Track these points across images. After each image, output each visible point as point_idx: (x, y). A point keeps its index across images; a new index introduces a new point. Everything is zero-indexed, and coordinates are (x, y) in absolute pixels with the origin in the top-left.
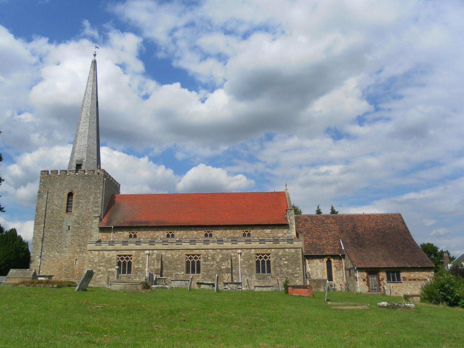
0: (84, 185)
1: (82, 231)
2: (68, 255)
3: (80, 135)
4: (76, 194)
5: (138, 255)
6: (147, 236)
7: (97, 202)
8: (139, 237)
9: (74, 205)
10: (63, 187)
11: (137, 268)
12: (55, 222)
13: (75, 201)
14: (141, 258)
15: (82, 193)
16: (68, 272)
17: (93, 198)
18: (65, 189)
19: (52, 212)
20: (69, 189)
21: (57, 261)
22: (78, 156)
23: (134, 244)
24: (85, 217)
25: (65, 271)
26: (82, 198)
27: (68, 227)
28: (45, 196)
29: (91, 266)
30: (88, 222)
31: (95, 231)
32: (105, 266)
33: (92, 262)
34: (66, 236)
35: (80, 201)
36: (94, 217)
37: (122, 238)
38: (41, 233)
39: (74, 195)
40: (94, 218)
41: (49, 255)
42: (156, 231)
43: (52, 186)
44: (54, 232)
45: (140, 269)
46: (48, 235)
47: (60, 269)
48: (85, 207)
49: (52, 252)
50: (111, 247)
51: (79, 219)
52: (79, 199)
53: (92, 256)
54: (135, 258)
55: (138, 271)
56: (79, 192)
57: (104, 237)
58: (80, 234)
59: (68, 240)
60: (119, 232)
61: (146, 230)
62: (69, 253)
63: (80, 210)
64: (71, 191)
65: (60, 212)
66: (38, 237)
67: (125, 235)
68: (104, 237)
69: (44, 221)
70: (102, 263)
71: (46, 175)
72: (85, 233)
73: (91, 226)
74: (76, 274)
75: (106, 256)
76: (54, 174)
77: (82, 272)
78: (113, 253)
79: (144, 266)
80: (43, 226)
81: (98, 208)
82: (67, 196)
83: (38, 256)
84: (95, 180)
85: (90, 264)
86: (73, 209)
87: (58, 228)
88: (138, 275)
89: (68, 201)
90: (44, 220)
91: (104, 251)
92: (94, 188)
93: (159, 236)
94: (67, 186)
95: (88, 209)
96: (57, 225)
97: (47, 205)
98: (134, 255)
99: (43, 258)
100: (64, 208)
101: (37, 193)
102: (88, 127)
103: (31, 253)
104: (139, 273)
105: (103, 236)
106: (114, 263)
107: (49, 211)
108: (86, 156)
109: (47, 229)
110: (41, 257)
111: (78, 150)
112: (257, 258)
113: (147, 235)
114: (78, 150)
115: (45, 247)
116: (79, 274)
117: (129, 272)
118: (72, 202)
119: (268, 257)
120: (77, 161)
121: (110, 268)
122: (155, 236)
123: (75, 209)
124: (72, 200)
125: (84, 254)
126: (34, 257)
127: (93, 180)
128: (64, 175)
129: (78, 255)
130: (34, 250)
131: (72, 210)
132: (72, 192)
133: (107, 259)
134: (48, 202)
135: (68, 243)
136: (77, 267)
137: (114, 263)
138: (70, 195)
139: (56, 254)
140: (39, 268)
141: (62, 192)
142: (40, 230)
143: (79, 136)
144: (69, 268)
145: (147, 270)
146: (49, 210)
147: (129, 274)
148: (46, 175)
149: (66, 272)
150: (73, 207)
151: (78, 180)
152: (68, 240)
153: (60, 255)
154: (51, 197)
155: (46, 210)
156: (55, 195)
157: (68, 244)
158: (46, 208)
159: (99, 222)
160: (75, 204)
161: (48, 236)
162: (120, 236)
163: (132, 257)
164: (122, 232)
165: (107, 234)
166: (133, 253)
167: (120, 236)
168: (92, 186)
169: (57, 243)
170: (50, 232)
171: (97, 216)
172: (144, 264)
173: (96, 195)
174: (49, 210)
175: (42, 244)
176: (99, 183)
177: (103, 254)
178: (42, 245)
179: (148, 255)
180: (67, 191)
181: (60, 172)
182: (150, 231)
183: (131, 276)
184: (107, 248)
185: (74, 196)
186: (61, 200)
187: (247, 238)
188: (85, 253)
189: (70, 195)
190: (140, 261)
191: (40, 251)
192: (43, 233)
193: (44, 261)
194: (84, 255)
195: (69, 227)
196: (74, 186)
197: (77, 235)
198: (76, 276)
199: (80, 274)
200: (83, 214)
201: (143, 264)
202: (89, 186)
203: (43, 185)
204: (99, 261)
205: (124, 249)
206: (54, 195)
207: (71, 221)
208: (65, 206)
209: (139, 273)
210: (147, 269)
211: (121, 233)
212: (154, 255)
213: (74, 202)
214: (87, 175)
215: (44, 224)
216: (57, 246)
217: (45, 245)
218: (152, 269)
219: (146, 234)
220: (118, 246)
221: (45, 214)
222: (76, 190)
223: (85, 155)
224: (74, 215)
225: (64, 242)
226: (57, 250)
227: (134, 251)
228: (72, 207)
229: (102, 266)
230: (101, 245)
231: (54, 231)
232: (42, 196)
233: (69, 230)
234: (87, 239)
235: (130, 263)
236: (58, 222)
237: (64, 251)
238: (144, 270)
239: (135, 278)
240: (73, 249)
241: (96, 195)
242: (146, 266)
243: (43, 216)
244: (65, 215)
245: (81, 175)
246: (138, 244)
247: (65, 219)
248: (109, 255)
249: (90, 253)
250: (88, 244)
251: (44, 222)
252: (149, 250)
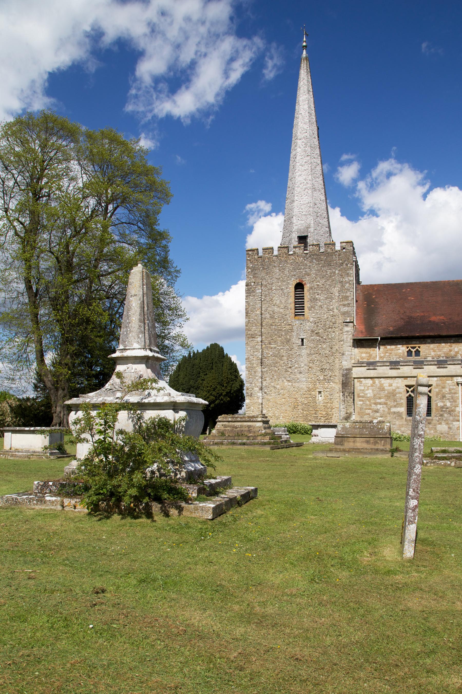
0: (321, 269)
3: (298, 187)
4: (308, 285)
9: (307, 305)
11: (442, 407)
13: (309, 297)
14: (447, 390)
15: (318, 283)
18: (288, 279)
19: (272, 317)
20: (296, 277)
22: (299, 222)
23: (435, 367)
24: (328, 323)
27: (300, 340)
29: (362, 404)
30: (334, 332)
32: (386, 404)
33: (363, 397)
34: (299, 355)
35: (317, 296)
39: (305, 287)
40: (345, 324)
41: (275, 386)
42: (453, 343)
43: (267, 274)
46: (269, 354)
47: (295, 408)
48: (325, 306)
50: (394, 373)
51: (318, 326)
52: (315, 293)
54: (437, 390)
55: (444, 411)
57: (364, 355)
59: (302, 362)
60: (389, 347)
61: (436, 342)
67: (400, 351)
68: (364, 355)
70: (380, 398)
71: (256, 257)
74: (321, 415)
75: (386, 388)
76: (269, 254)
77: (331, 413)
79: (453, 403)
82: (293, 290)
84: (339, 260)
86: (306, 310)
88: (444, 419)
91: (381, 379)
92: (339, 274)
93: (458, 351)
94: (292, 273)
95: (332, 310)
98: (434, 385)
99: (266, 391)
101: (245, 286)
102: (310, 173)
103: (245, 382)
104: (446, 415)
105: (362, 353)
106: (401, 399)
109: (266, 345)
110: (261, 389)
111: (298, 213)
114: (298, 213)
118: (304, 299)
120: (298, 231)
121: (395, 406)
122: (451, 352)
123: (310, 310)
125: (331, 383)
128: (286, 254)
131: (304, 312)
133: (389, 393)
134: (264, 300)
135: (302, 366)
138: (299, 286)
139: (286, 384)
140: (260, 407)
142: (257, 347)
143: (296, 188)
149: (305, 412)
150: (305, 308)
151: (310, 262)
152: (304, 360)
156: (274, 288)
157: (303, 368)
161: (269, 355)
162: (390, 354)
164: (393, 347)
165: (368, 350)
167: (390, 354)
169: (285, 367)
173: (343, 286)
176: (347, 265)
177: (382, 385)
180: (293, 282)
181: (278, 251)
182: (443, 344)
183: (432, 420)
185: (305, 289)
187: (414, 358)
189: (299, 286)
193: (267, 395)
195: (302, 340)
198: (321, 419)
203: (253, 273)
204: (374, 396)
206: (272, 289)
209: (446, 415)
211: (392, 349)
214: (323, 252)
216: (287, 371)
219: (435, 349)
223: (311, 221)
226: (287, 378)
227: (435, 379)
228: (304, 307)
229: (380, 404)
231: (277, 347)
232: (253, 291)
233: (303, 345)
236: (283, 333)
241: (343, 286)
243: (258, 323)
247: (295, 328)
248: (392, 386)
249: (358, 382)
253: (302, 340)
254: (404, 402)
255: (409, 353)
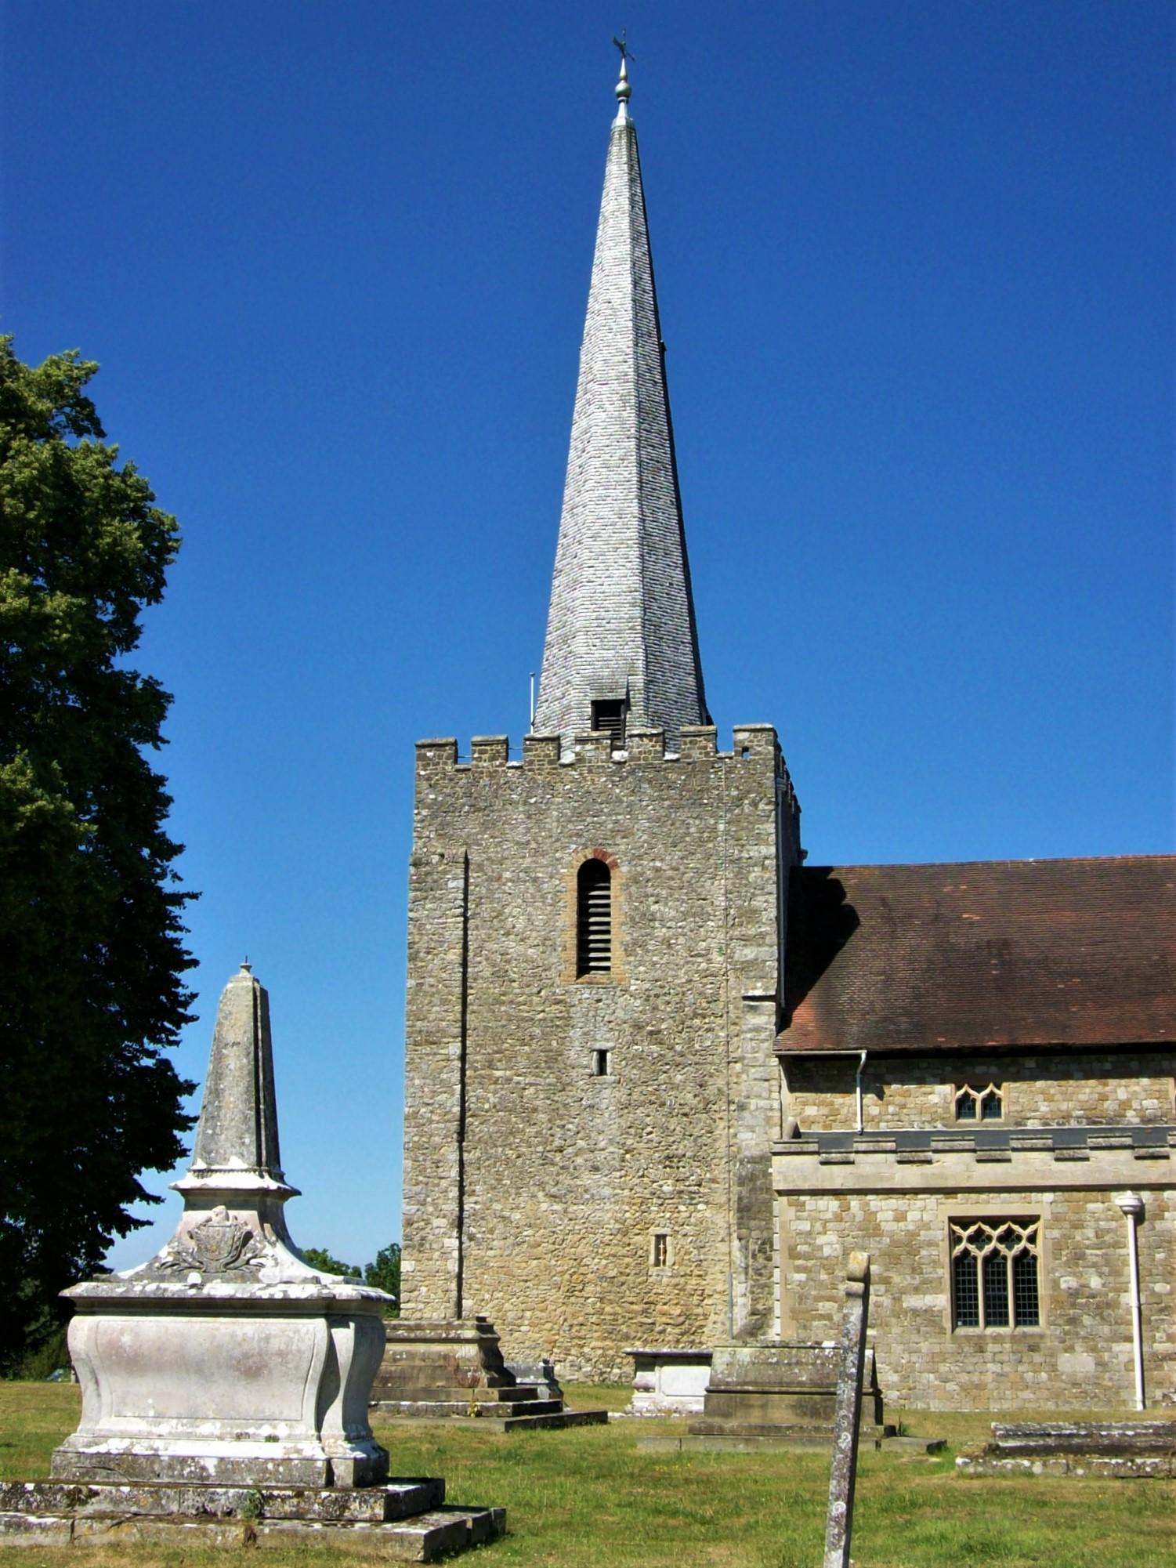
1: (679, 1077)
2: (609, 1215)
4: (624, 869)
5: (1073, 1217)
6: (1064, 1106)
7: (752, 915)
8: (1013, 1108)
9: (619, 935)
10: (550, 830)
11: (1074, 1294)
12: (518, 1027)
13: (626, 908)
14: (1091, 1233)
15: (658, 864)
16: (618, 1310)
17: (727, 892)
19: (501, 975)
21: (551, 1247)
25: (601, 1300)
26: (664, 893)
28: (451, 884)
30: (708, 1030)
31: (757, 1076)
34: (591, 1106)
36: (746, 998)
37: (917, 1119)
38: (447, 1086)
39: (613, 873)
40: (747, 1003)
41: (506, 1214)
43: (485, 826)
44: (518, 1083)
45: (1094, 1297)
47: (571, 1292)
48: (681, 940)
49: (518, 1194)
50: (911, 1176)
52: (647, 896)
53: (805, 1226)
54: (1056, 1233)
56: (640, 857)
57: (811, 1111)
58: (669, 1097)
62: (616, 1202)
63: (655, 964)
64: (595, 851)
65: (545, 970)
66: (432, 1112)
67: (934, 1099)
69: (459, 1024)
71: (448, 768)
72: (697, 1090)
73: (727, 1051)
74: (664, 1319)
76: (493, 758)
77: (699, 1310)
78: (923, 1209)
80: (459, 1052)
81: (759, 945)
82: (573, 883)
83: (444, 1217)
85: (798, 1272)
86: (616, 952)
87: (543, 1065)
88: (1082, 1333)
89: (583, 911)
90: (459, 1016)
91: (869, 1197)
92: (727, 832)
94: (570, 826)
95: (706, 955)
96: (534, 1046)
97: (466, 935)
98: (1046, 1215)
99: (473, 1230)
100: (565, 949)
104: (1087, 1320)
105: (805, 1104)
106: (935, 1263)
107: (480, 967)
108: (641, 655)
110: (460, 1223)
112: (959, 1240)
113: (1058, 1097)
115: (479, 1169)
116: (682, 1319)
117: (1027, 1312)
119: (1025, 1233)
121: (916, 1290)
122: (1106, 1104)
123: (629, 951)
124: (608, 906)
125: (701, 1207)
126: (422, 1224)
127: (717, 788)
129: (668, 1215)
130: (417, 1184)
132: (599, 857)
135: (602, 1145)
136: (665, 1280)
137: (934, 1262)
141: (544, 861)
142: (444, 1076)
144: (623, 1284)
145: (1134, 1303)
146: (479, 959)
147: (1025, 1323)
148: (445, 763)
149: (608, 1309)
153: (566, 1211)
154: (484, 891)
155: (465, 964)
157: (604, 1154)
158: (465, 949)
159: (774, 1028)
160: (624, 928)
162: (903, 1106)
163: (1036, 1232)
166: (1042, 1204)
167: (903, 1106)
168: (712, 821)
169: (540, 1149)
170: (496, 1083)
171: (758, 993)
172: (1112, 1269)
174: (479, 959)
175: (461, 1150)
176: (755, 804)
177: (870, 1215)
178: (461, 1155)
179: (1130, 1216)
184: (891, 1178)
185: (614, 883)
186: (543, 902)
188: (707, 1203)
190: (1088, 1252)
191: (454, 1192)
192: (458, 1087)
194: (699, 1215)
195: (602, 1054)
196: (610, 826)
197: (652, 1103)
199: (688, 1317)
200: (677, 981)
201: (1106, 1270)
202: (697, 822)
205: (987, 1184)
206: (499, 878)
207: (611, 1025)
208: (570, 937)
210: (1131, 1299)
212: (1166, 1214)
213: (616, 917)
215: (464, 1042)
216: (546, 1161)
217: (479, 1159)
218: (1159, 1295)
220: (954, 1167)
221: (459, 983)
222: (622, 845)
224: (625, 991)
225: (582, 1143)
227: (1048, 1197)
230: (853, 1163)
233: (602, 1071)
234: (710, 1125)
235: (1026, 1264)
236: (538, 1031)
237: (586, 1191)
238: (1113, 1305)
239: (1066, 1351)
240: (638, 1181)
241: (739, 875)
242: (1123, 1279)
244: (573, 988)
245: (645, 759)
246: (1066, 1153)
247: (577, 1013)
248: (905, 1219)
249: (790, 1204)
250: (775, 1159)
251: (460, 1030)
252: (1136, 1188)
253: (602, 1054)
254: (944, 1273)
255: (964, 1106)
